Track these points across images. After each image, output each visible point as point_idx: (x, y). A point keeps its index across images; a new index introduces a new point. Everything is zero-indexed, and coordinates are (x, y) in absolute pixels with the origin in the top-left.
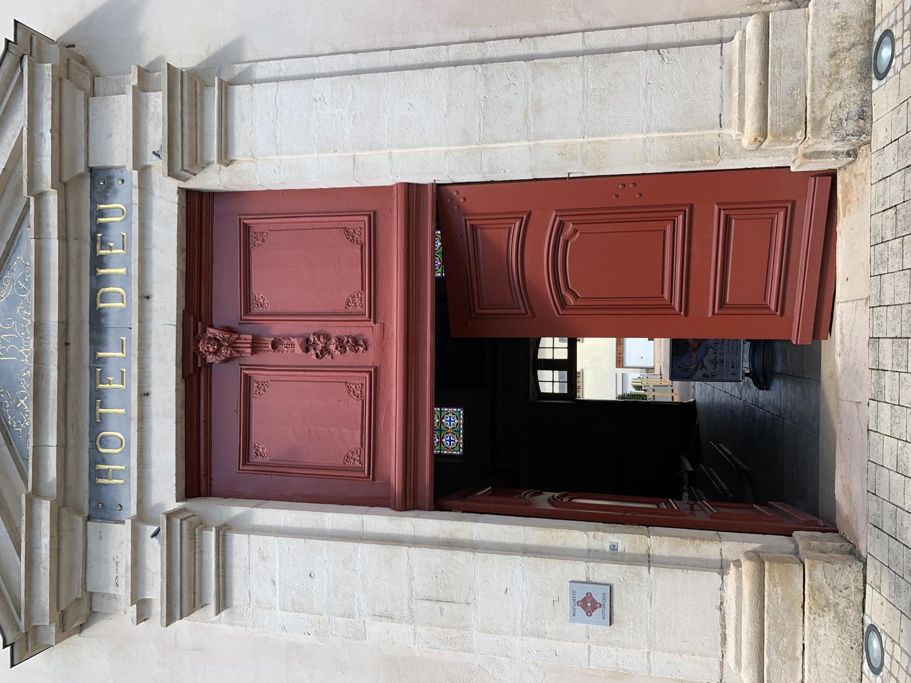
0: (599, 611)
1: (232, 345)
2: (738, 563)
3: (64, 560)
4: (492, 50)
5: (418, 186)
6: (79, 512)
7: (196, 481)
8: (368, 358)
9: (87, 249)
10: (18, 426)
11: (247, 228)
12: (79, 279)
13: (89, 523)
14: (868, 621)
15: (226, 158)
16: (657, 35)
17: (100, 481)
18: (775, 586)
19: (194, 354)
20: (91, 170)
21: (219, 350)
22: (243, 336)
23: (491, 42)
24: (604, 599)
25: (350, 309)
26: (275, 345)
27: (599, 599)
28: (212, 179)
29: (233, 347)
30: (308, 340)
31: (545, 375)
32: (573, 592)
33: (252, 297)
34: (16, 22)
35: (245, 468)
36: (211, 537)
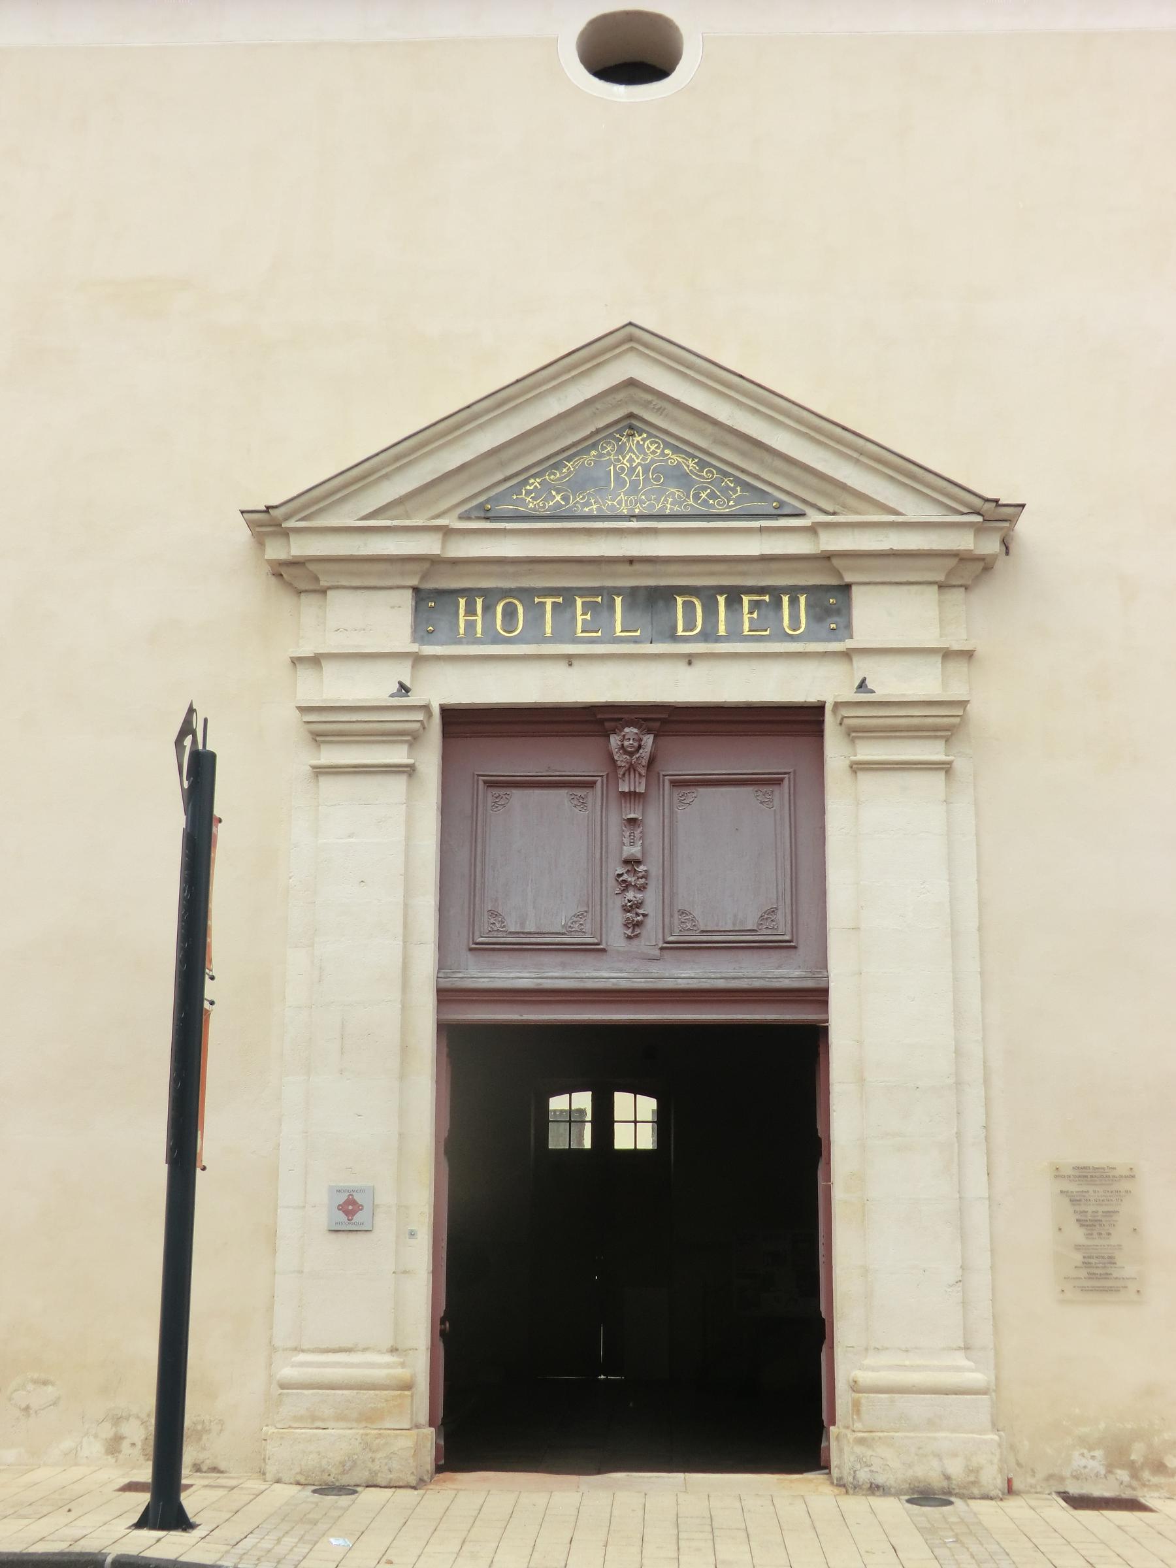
0: (342, 1217)
1: (631, 768)
2: (403, 1365)
3: (366, 567)
5: (826, 1003)
6: (424, 577)
7: (462, 723)
8: (615, 937)
9: (750, 582)
10: (528, 493)
11: (778, 782)
12: (712, 574)
13: (411, 591)
14: (359, 1489)
15: (857, 768)
18: (387, 1401)
19: (621, 719)
20: (847, 588)
21: (626, 752)
22: (643, 781)
23: (983, 1093)
24: (357, 1224)
25: (676, 916)
26: (632, 821)
27: (358, 1218)
28: (837, 752)
29: (629, 770)
30: (639, 863)
31: (623, 1139)
32: (362, 1191)
33: (693, 789)
34: (1023, 506)
35: (481, 783)
36: (397, 755)
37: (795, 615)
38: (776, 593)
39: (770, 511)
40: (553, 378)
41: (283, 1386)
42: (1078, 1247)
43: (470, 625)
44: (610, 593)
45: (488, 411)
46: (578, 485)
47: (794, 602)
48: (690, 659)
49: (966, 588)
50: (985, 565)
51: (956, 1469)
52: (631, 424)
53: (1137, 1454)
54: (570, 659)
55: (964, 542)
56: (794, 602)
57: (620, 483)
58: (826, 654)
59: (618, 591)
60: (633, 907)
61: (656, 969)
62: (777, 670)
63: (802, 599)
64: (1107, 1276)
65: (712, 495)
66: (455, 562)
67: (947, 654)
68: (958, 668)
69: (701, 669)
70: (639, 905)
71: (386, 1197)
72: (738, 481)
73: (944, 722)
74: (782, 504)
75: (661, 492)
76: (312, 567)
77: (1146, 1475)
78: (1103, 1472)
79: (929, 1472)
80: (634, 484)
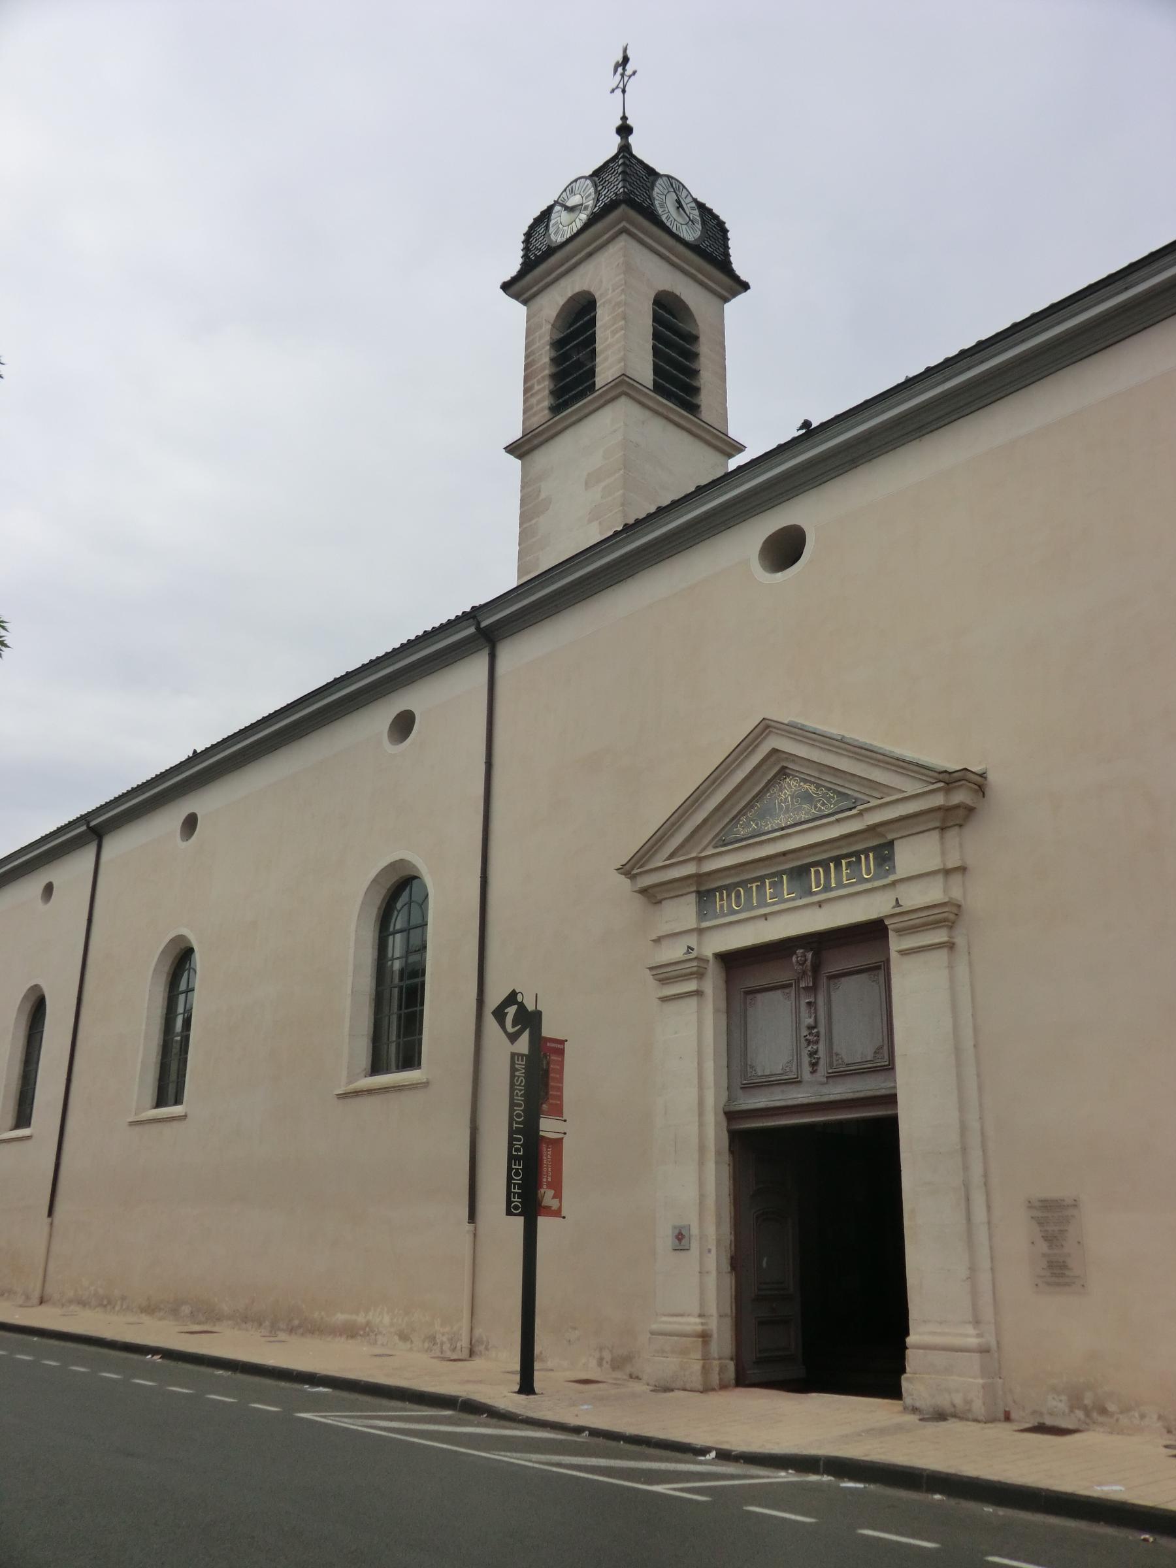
4: (976, 1154)
5: (896, 1102)
6: (699, 884)
7: (731, 961)
9: (845, 851)
12: (825, 851)
15: (903, 953)
16: (985, 1279)
17: (832, 865)
20: (891, 843)
27: (683, 1242)
28: (896, 944)
36: (692, 986)
37: (867, 866)
38: (857, 854)
39: (849, 805)
40: (736, 760)
41: (652, 1333)
42: (1044, 1255)
43: (722, 906)
44: (779, 874)
45: (709, 787)
46: (762, 816)
47: (867, 857)
48: (820, 904)
49: (960, 826)
50: (970, 810)
51: (958, 1400)
52: (783, 773)
53: (1088, 1401)
54: (765, 917)
55: (939, 800)
56: (867, 857)
57: (781, 808)
58: (884, 886)
59: (784, 872)
60: (812, 1054)
61: (825, 1090)
62: (862, 901)
63: (871, 855)
64: (1063, 1275)
65: (823, 805)
66: (709, 874)
67: (947, 872)
68: (956, 879)
69: (826, 908)
70: (816, 1052)
71: (695, 1231)
72: (835, 792)
73: (946, 916)
74: (856, 799)
75: (799, 809)
76: (879, 830)
77: (1095, 1415)
78: (1067, 1411)
79: (943, 1401)
80: (787, 807)
